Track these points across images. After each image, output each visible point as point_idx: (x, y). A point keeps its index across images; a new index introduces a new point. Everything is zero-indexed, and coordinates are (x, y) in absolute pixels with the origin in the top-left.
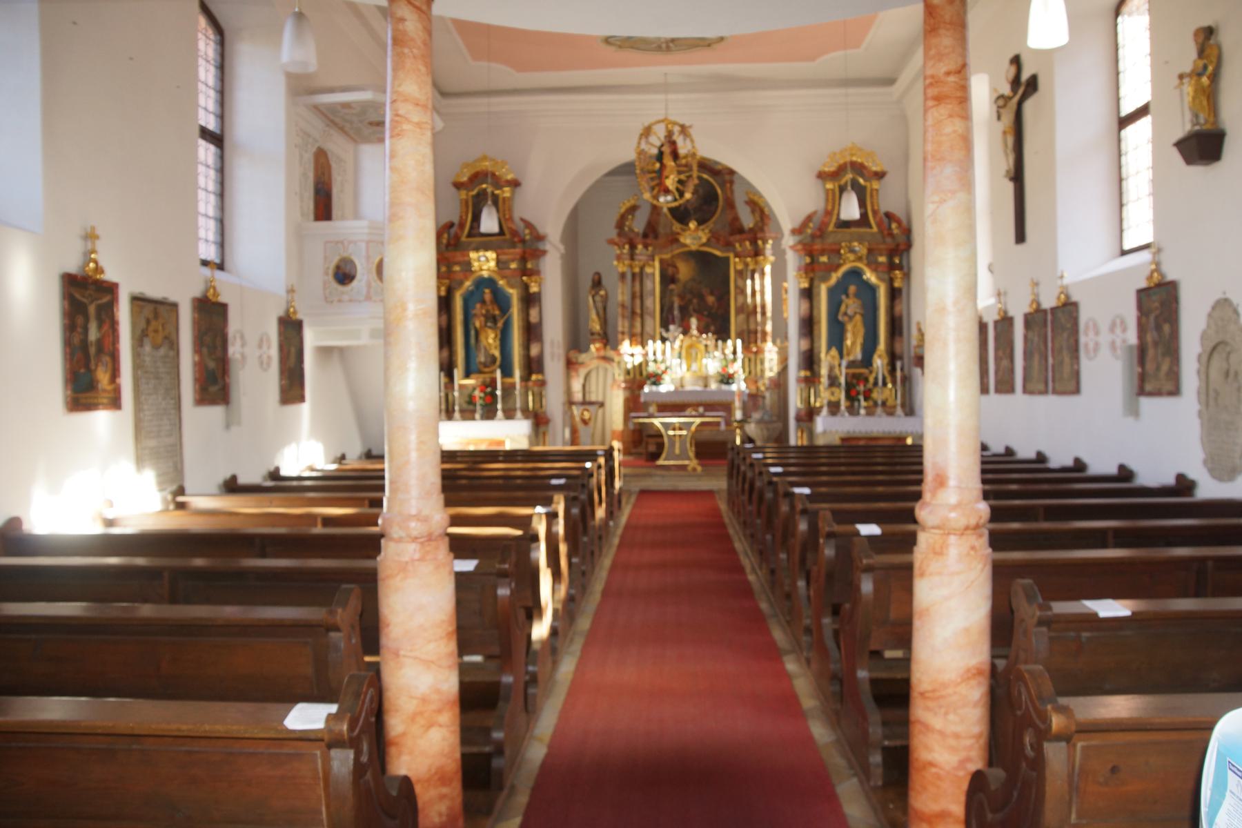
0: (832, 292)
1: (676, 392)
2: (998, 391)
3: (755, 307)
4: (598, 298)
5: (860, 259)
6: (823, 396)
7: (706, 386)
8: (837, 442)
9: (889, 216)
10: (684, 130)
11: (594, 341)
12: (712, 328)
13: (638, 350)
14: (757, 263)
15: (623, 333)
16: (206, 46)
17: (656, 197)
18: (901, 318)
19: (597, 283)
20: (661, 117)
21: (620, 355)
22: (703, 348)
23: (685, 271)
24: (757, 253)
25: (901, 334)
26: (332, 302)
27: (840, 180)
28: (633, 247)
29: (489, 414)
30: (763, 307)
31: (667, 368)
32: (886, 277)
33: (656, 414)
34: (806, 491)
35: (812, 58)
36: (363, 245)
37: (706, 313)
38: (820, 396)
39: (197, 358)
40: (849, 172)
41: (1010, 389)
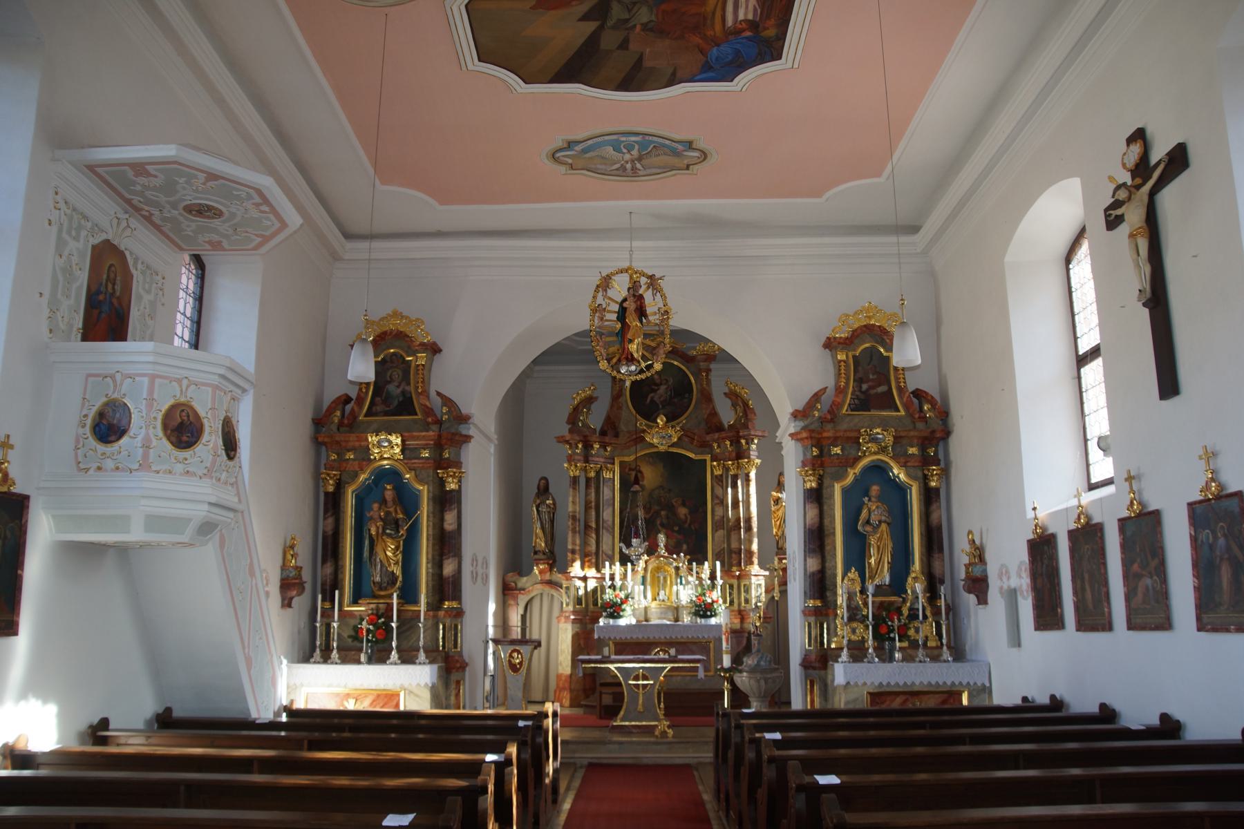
0: (846, 492)
1: (639, 626)
2: (1082, 626)
3: (738, 520)
4: (543, 509)
5: (883, 450)
6: (841, 634)
7: (677, 620)
8: (864, 703)
9: (919, 394)
10: (653, 281)
11: (537, 562)
12: (685, 547)
13: (591, 572)
15: (573, 552)
16: (187, 280)
17: (616, 367)
18: (940, 528)
19: (544, 490)
20: (626, 264)
21: (570, 578)
23: (651, 476)
24: (740, 455)
25: (941, 550)
26: (87, 470)
27: (855, 350)
28: (588, 446)
29: (379, 657)
30: (748, 520)
31: (627, 597)
32: (920, 474)
33: (613, 657)
34: (777, 736)
35: (817, 193)
36: (146, 380)
37: (676, 528)
38: (836, 635)
39: (19, 572)
41: (1106, 625)
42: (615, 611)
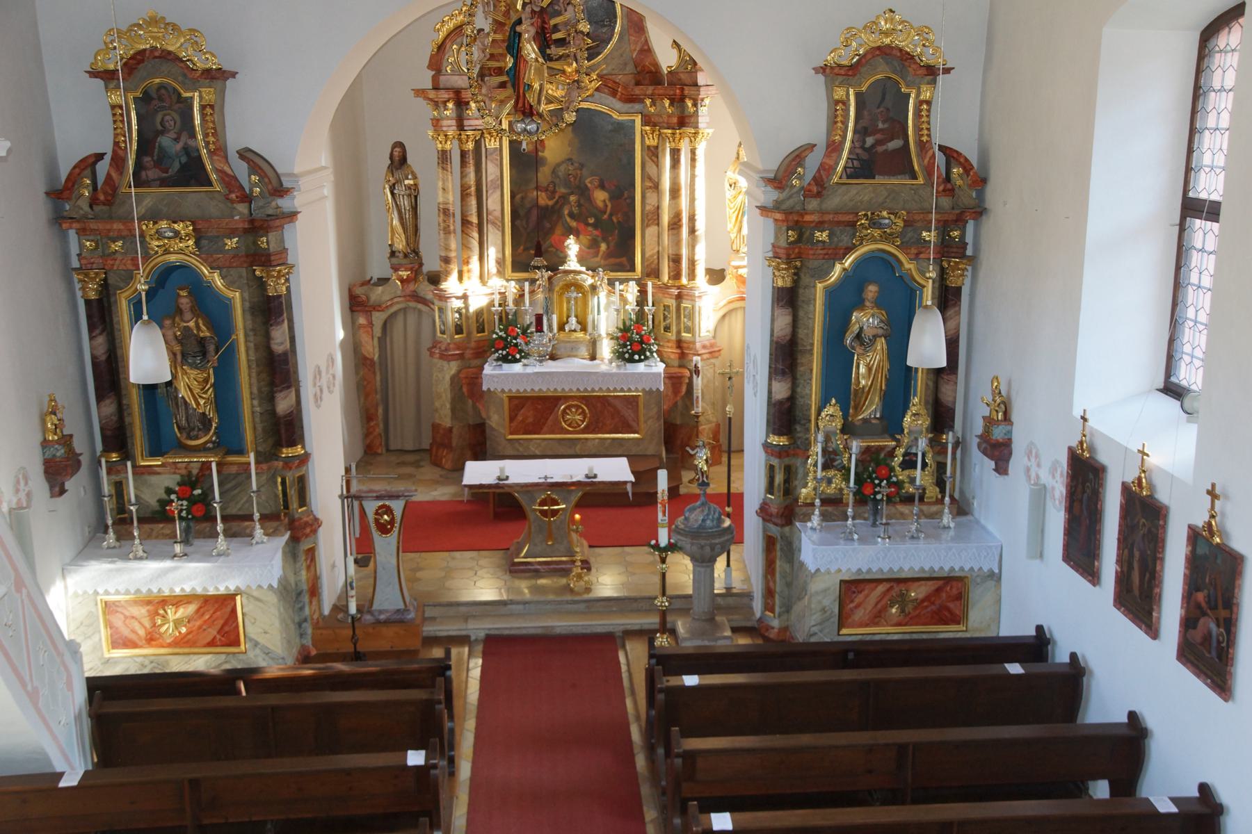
5: (887, 238)
19: (399, 160)
42: (508, 354)
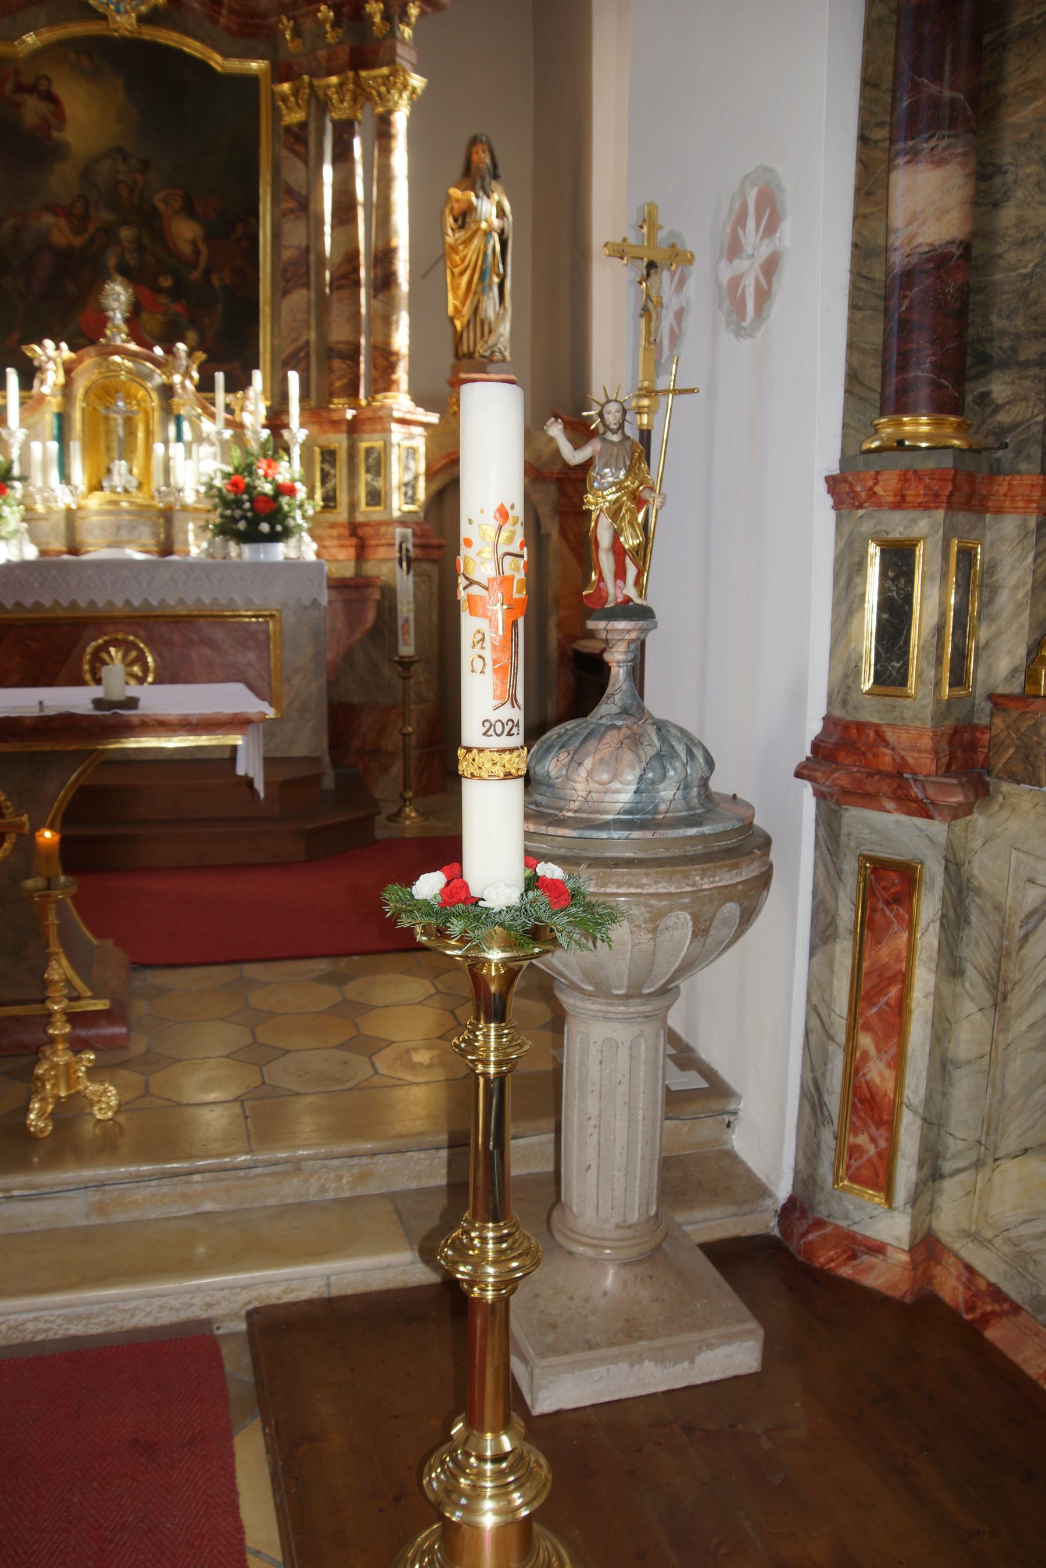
3: (351, 258)
7: (166, 549)
14: (361, 95)
22: (155, 401)
37: (166, 282)
40: (779, 1235)
